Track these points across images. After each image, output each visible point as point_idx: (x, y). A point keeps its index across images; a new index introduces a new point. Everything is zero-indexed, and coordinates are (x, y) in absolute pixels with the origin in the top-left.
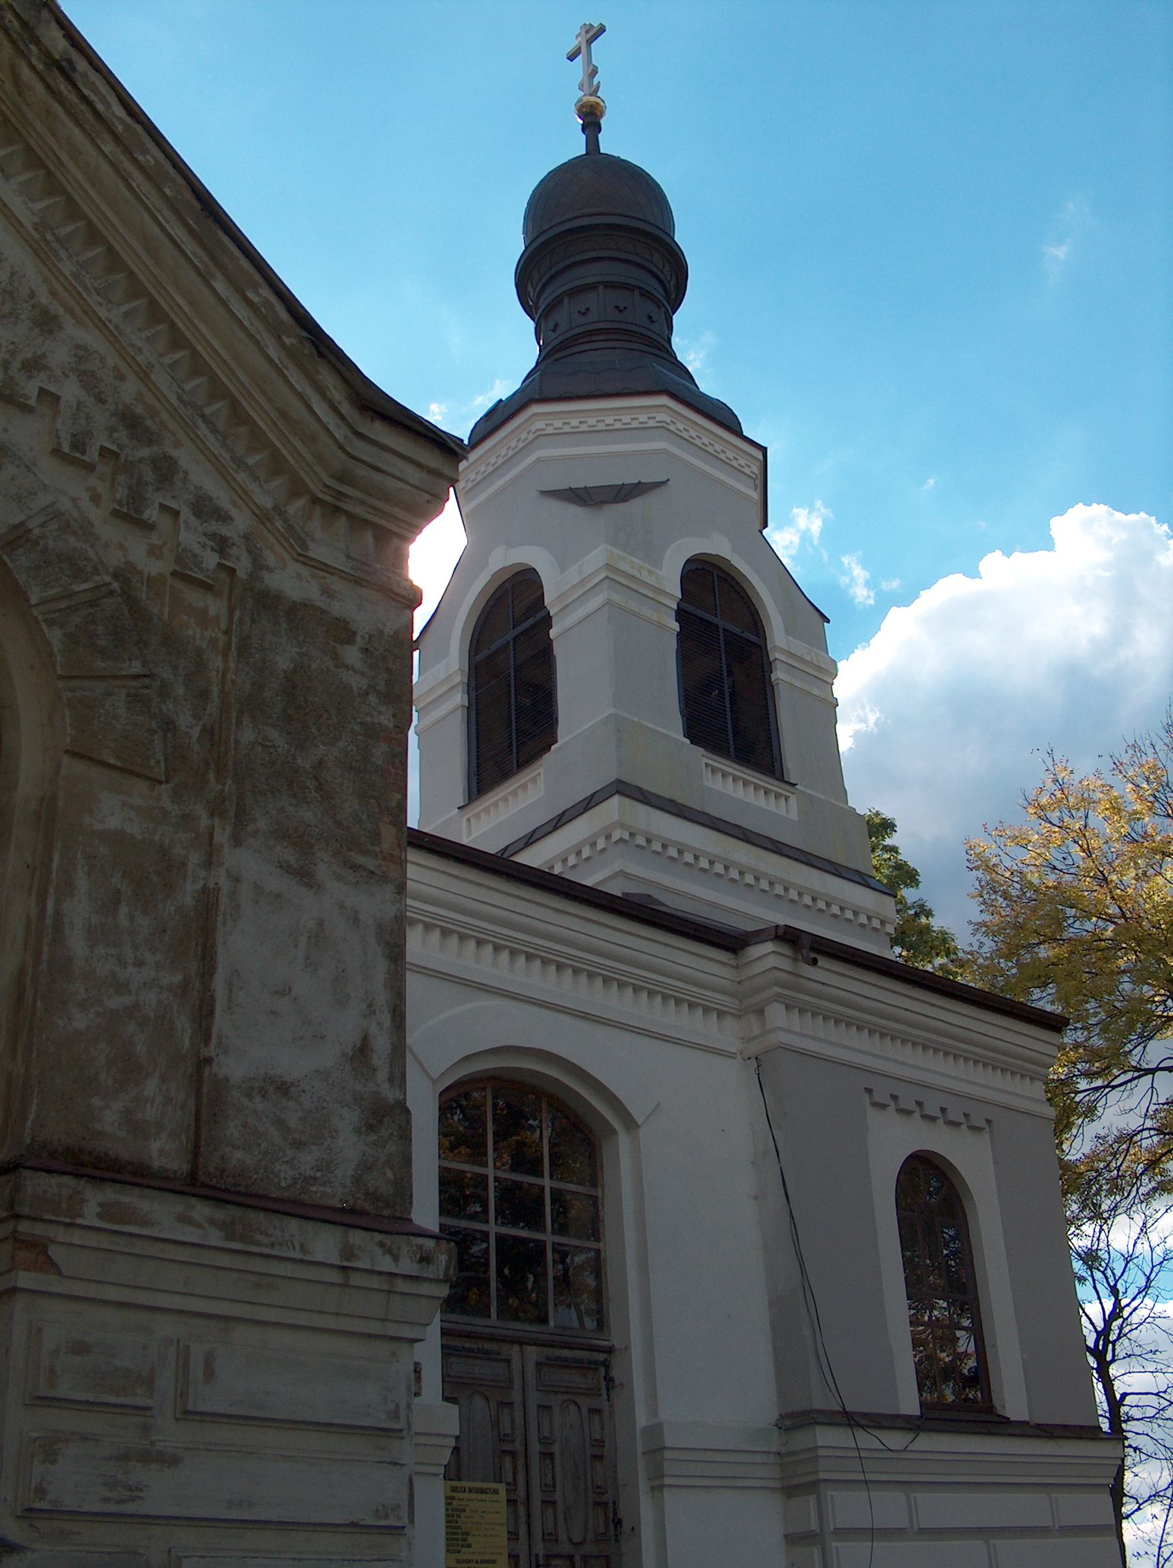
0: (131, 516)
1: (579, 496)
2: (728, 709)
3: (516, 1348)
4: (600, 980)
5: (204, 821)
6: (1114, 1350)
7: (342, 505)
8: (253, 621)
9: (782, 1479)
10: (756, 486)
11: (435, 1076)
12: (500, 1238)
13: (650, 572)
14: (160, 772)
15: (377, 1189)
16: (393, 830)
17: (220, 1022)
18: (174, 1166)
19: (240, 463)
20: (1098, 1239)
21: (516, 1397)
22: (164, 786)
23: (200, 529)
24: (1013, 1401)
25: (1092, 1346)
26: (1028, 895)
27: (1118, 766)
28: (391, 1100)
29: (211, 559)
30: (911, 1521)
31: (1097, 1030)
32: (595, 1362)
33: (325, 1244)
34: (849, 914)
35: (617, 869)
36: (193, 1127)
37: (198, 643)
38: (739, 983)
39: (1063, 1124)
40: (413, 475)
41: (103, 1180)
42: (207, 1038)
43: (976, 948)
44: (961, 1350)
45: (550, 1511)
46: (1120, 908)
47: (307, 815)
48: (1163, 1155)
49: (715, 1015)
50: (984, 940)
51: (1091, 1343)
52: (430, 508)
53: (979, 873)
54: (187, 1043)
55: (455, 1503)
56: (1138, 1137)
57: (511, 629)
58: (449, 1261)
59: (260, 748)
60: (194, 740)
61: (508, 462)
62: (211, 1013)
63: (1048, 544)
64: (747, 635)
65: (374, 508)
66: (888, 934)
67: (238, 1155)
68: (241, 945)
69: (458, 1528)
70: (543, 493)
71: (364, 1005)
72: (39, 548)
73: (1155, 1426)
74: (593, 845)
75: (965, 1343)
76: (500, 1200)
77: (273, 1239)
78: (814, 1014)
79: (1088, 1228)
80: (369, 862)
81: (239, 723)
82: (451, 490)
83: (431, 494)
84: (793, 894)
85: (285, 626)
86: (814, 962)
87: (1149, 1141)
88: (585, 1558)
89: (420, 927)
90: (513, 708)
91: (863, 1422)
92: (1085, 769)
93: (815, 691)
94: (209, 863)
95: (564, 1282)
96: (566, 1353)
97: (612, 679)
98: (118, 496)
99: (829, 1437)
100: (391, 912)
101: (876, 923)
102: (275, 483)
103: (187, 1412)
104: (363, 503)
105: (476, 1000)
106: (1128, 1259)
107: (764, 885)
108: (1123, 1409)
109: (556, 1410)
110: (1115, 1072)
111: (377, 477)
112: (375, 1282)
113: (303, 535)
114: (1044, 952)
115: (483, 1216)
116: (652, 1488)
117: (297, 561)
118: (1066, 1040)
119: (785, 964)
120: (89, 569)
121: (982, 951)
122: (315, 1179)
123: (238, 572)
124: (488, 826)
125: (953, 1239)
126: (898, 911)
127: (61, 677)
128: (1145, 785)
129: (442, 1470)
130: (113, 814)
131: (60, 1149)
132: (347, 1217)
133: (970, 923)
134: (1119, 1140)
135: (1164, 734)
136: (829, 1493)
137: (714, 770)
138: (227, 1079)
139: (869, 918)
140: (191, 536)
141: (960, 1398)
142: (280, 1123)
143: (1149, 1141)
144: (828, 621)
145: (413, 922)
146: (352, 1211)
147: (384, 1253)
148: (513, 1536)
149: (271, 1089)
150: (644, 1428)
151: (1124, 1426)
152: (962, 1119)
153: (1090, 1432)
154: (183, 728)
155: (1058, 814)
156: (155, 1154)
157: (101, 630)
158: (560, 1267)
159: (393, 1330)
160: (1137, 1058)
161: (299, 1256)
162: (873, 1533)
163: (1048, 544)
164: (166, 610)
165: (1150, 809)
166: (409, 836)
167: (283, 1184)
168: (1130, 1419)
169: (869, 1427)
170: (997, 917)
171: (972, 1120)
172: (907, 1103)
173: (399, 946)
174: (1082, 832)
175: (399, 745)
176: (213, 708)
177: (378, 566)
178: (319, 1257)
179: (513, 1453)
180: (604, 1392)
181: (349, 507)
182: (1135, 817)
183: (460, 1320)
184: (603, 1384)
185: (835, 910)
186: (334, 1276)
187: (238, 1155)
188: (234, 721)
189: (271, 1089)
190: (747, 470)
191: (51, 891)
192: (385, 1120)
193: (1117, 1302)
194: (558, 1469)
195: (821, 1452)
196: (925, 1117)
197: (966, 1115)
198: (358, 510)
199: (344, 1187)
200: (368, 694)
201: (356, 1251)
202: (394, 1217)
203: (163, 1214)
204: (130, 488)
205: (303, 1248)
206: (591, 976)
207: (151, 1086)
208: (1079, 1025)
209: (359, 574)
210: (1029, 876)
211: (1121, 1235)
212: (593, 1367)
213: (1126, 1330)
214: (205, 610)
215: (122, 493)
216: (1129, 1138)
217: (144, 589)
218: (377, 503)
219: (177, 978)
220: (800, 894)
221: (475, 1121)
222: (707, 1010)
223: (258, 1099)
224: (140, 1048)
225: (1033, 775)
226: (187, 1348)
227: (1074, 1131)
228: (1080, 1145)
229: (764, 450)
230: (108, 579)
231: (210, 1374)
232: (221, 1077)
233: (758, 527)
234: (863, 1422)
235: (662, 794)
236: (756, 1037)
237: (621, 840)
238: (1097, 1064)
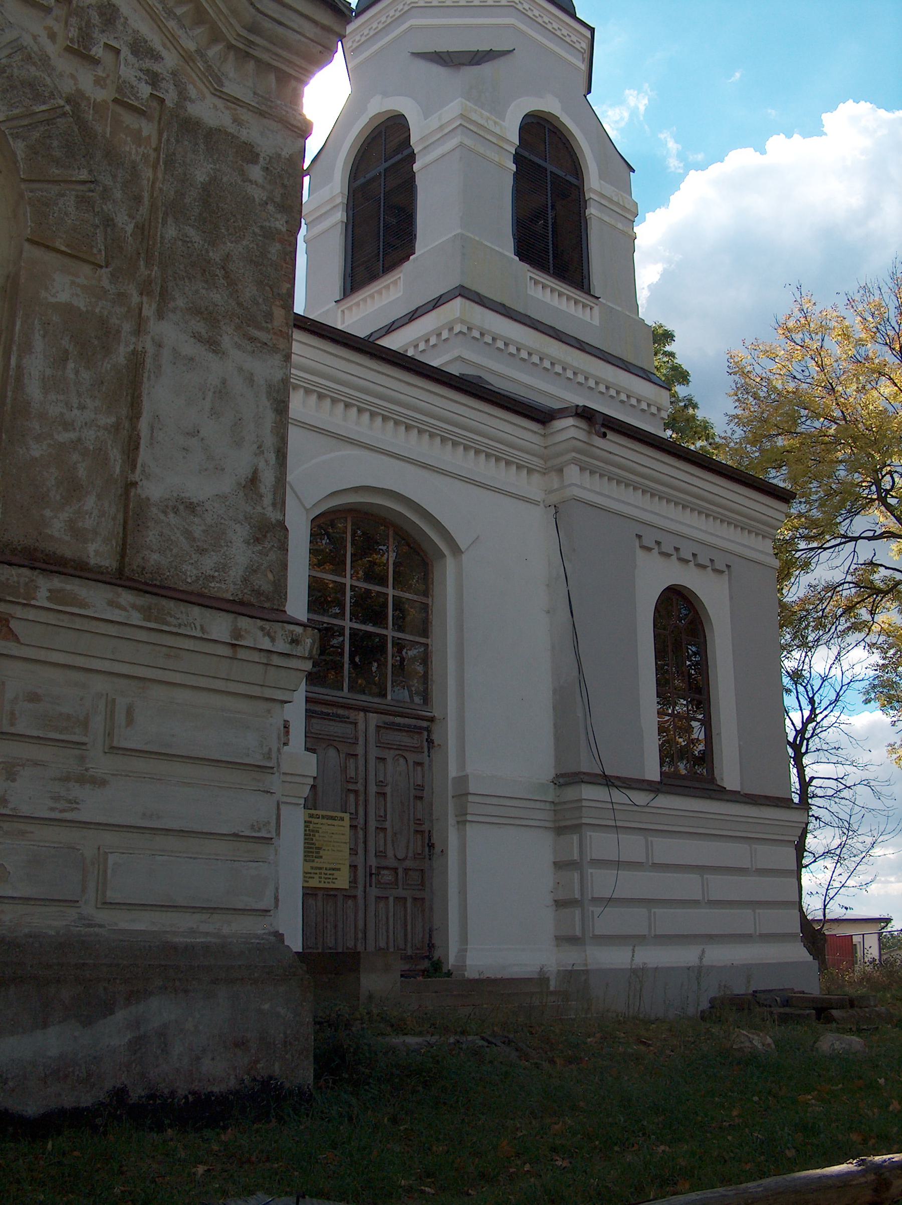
0: (80, 52)
1: (441, 57)
2: (550, 236)
3: (362, 714)
4: (438, 439)
5: (135, 299)
6: (807, 745)
7: (251, 51)
8: (177, 141)
9: (555, 821)
10: (584, 61)
11: (308, 507)
12: (354, 633)
13: (495, 123)
14: (101, 259)
15: (260, 586)
16: (283, 312)
17: (144, 455)
18: (106, 563)
19: (170, 13)
20: (803, 662)
21: (360, 750)
22: (104, 270)
23: (137, 65)
24: (730, 776)
25: (791, 741)
26: (773, 397)
27: (851, 302)
28: (274, 521)
29: (145, 90)
30: (647, 857)
31: (817, 504)
32: (421, 728)
33: (220, 626)
34: (633, 401)
35: (457, 355)
36: (121, 535)
37: (133, 157)
38: (545, 447)
39: (784, 574)
40: (310, 30)
41: (52, 572)
42: (133, 467)
43: (729, 434)
44: (695, 736)
45: (382, 835)
46: (842, 412)
47: (217, 297)
48: (858, 603)
49: (525, 472)
50: (735, 428)
51: (791, 739)
52: (322, 57)
53: (736, 378)
54: (118, 470)
55: (311, 826)
56: (841, 588)
57: (384, 167)
58: (314, 642)
59: (180, 243)
60: (129, 234)
61: (387, 28)
62: (137, 448)
63: (817, 130)
64: (569, 178)
65: (277, 55)
66: (663, 419)
67: (155, 556)
68: (161, 396)
69: (313, 844)
70: (413, 54)
71: (255, 446)
72: (5, 75)
73: (833, 803)
74: (439, 335)
75: (698, 732)
76: (354, 605)
77: (180, 621)
78: (601, 476)
79: (797, 654)
80: (263, 336)
81: (164, 223)
82: (340, 43)
83: (323, 46)
84: (591, 383)
85: (202, 146)
86: (604, 435)
87: (849, 592)
88: (406, 870)
89: (302, 391)
90: (382, 225)
91: (617, 783)
92: (827, 304)
93: (620, 226)
94: (139, 330)
95: (400, 667)
96: (398, 720)
97: (462, 209)
98: (70, 35)
99: (591, 793)
100: (279, 375)
101: (654, 410)
102: (198, 31)
103: (112, 748)
104: (268, 50)
105: (342, 450)
106: (824, 679)
107: (569, 374)
108: (811, 789)
109: (389, 761)
110: (828, 537)
111: (280, 30)
112: (256, 657)
113: (219, 74)
114: (781, 442)
115: (342, 615)
116: (458, 822)
117: (215, 95)
118: (792, 511)
119: (582, 435)
120: (47, 94)
121: (734, 437)
122: (213, 577)
123: (166, 102)
124: (359, 316)
125: (695, 654)
126: (672, 403)
127: (24, 180)
128: (870, 319)
129: (302, 801)
130: (63, 291)
131: (19, 548)
132: (237, 607)
133: (726, 414)
134: (827, 589)
135: (889, 280)
136: (589, 833)
137: (536, 282)
138: (148, 499)
139: (649, 405)
140: (129, 71)
141: (689, 769)
142: (188, 534)
143: (849, 592)
144: (634, 171)
145: (296, 387)
146: (242, 603)
147: (264, 636)
148: (353, 852)
149: (181, 508)
150: (454, 778)
151: (810, 801)
152: (708, 563)
153: (784, 803)
154: (120, 224)
155: (801, 336)
156: (92, 554)
157: (55, 143)
158: (398, 658)
159: (268, 693)
160: (845, 529)
161: (199, 634)
162: (618, 864)
163: (817, 130)
164: (108, 130)
165: (873, 338)
166: (295, 319)
167: (189, 580)
168: (815, 796)
169: (621, 787)
170: (747, 412)
171: (717, 565)
172: (667, 548)
173: (284, 402)
174: (819, 351)
175: (290, 245)
176: (144, 210)
177: (279, 102)
178: (214, 637)
179: (356, 792)
180: (426, 750)
181: (255, 53)
182: (860, 343)
183: (322, 692)
184: (425, 744)
185: (623, 397)
186: (227, 651)
187: (155, 556)
188: (160, 221)
189: (181, 508)
190: (577, 46)
191: (15, 348)
192: (268, 535)
193: (813, 710)
194: (389, 805)
195: (584, 803)
196: (680, 559)
197: (712, 561)
198: (265, 57)
199: (235, 584)
200: (267, 204)
201: (243, 633)
202: (272, 609)
203: (97, 598)
204: (80, 29)
205: (202, 629)
206: (432, 435)
207: (90, 502)
208: (803, 500)
209: (264, 108)
210: (774, 383)
211: (820, 661)
212: (418, 731)
213: (818, 731)
214: (140, 131)
215: (73, 33)
216: (833, 588)
217: (91, 112)
218: (280, 51)
219: (112, 420)
220: (597, 383)
221: (337, 543)
222: (519, 467)
223: (171, 515)
224: (82, 472)
225: (784, 305)
226: (114, 700)
227: (792, 580)
228: (796, 590)
229: (592, 30)
230: (62, 103)
231: (130, 720)
232: (143, 496)
233: (584, 92)
234: (617, 783)
235: (495, 299)
236: (557, 490)
237: (460, 332)
238: (814, 531)
